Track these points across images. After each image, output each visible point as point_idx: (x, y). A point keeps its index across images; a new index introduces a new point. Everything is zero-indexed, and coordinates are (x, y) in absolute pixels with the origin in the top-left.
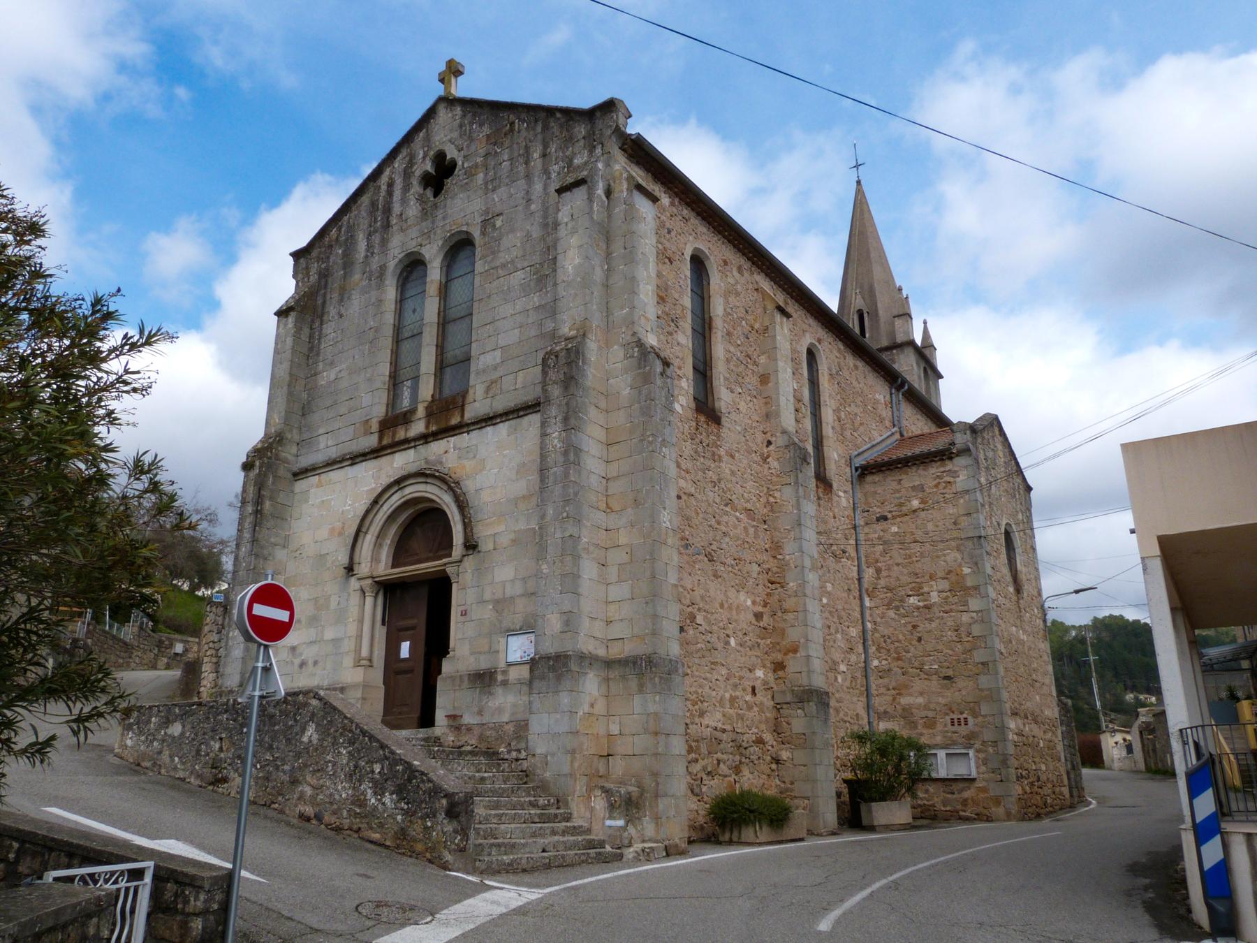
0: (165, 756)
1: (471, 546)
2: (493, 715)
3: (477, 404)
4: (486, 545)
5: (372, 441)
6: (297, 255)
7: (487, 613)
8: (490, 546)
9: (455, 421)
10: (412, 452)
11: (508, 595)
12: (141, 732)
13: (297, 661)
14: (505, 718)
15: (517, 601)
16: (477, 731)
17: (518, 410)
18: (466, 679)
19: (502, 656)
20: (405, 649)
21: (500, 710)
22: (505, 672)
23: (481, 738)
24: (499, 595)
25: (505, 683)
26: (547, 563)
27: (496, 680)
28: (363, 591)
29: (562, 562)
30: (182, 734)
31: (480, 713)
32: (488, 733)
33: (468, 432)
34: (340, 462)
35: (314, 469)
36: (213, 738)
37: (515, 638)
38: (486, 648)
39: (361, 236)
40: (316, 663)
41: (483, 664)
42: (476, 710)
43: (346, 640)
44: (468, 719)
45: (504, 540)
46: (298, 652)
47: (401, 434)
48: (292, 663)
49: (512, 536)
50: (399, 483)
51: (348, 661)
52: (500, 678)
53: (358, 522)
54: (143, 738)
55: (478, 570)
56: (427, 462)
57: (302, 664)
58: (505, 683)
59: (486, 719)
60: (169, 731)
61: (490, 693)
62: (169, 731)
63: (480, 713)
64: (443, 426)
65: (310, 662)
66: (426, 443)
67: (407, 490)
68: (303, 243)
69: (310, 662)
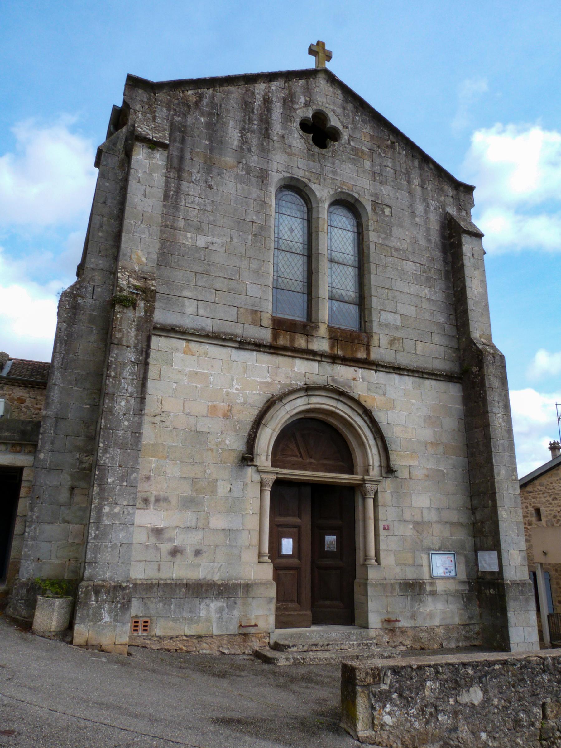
0: (464, 732)
1: (389, 470)
2: (425, 619)
3: (381, 350)
4: (403, 474)
5: (265, 335)
6: (133, 83)
7: (409, 531)
8: (406, 476)
9: (361, 355)
10: (316, 364)
11: (426, 519)
12: (407, 702)
13: (165, 548)
14: (437, 622)
15: (434, 525)
16: (410, 633)
17: (423, 373)
18: (397, 586)
19: (426, 569)
20: (287, 546)
21: (431, 615)
22: (432, 584)
23: (416, 639)
24: (418, 518)
25: (433, 593)
26: (506, 510)
27: (425, 589)
28: (262, 484)
29: (516, 512)
30: (487, 701)
31: (413, 617)
32: (422, 635)
33: (376, 371)
34: (224, 340)
35: (184, 333)
36: (534, 704)
37: (437, 556)
38: (410, 561)
39: (231, 123)
40: (198, 553)
41: (410, 575)
42: (409, 614)
43: (245, 534)
44: (404, 623)
45: (419, 473)
46: (166, 536)
47: (301, 342)
48: (157, 548)
49: (426, 472)
50: (309, 389)
51: (250, 556)
52: (428, 588)
53: (255, 412)
54: (413, 711)
55: (397, 494)
56: (333, 380)
57: (175, 552)
58: (433, 593)
59: (419, 622)
60: (464, 698)
61: (421, 601)
62: (464, 698)
63: (413, 617)
64: (349, 355)
65: (189, 551)
66: (333, 363)
67: (314, 400)
68: (154, 77)
69: (189, 551)
